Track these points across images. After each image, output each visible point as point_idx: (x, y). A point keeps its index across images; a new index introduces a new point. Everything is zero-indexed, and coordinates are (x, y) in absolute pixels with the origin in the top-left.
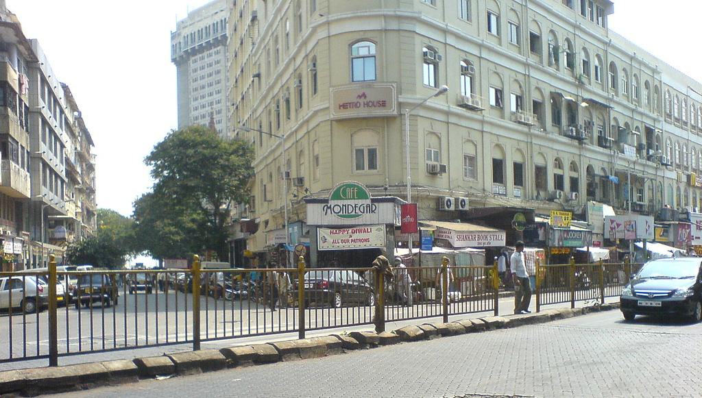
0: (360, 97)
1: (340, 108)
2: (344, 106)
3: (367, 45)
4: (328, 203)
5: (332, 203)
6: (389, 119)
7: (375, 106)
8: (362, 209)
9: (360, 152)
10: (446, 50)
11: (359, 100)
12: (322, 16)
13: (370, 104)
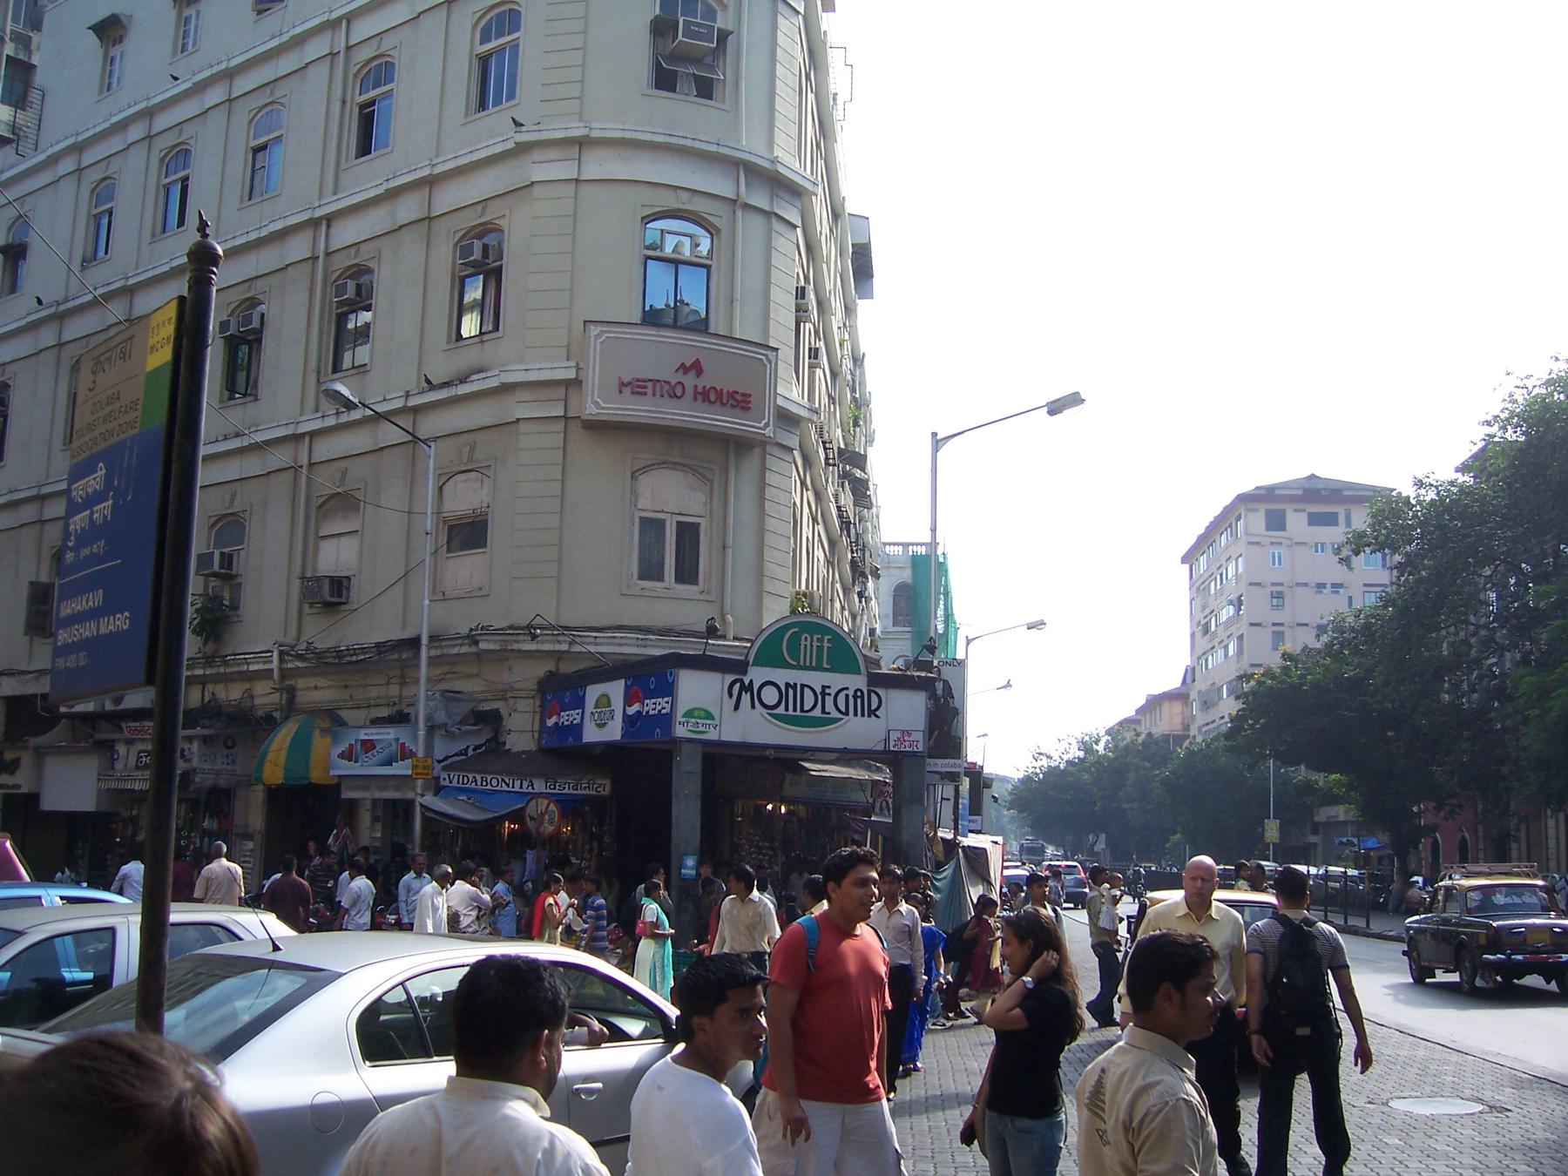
0: (684, 369)
1: (695, 399)
2: (637, 387)
3: (690, 232)
4: (745, 673)
5: (757, 675)
6: (737, 446)
7: (723, 404)
8: (842, 705)
9: (652, 527)
10: (338, 250)
11: (680, 377)
12: (176, 79)
13: (713, 397)
